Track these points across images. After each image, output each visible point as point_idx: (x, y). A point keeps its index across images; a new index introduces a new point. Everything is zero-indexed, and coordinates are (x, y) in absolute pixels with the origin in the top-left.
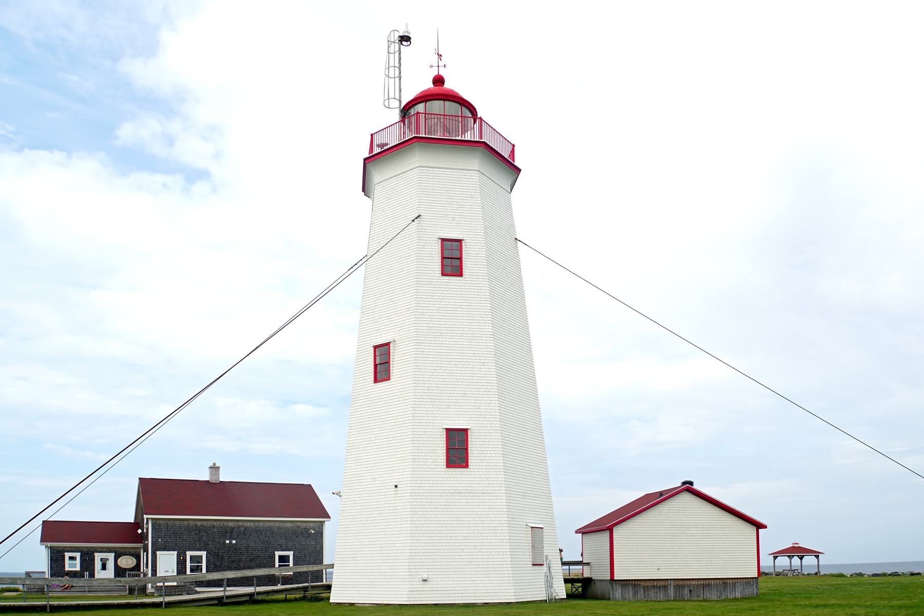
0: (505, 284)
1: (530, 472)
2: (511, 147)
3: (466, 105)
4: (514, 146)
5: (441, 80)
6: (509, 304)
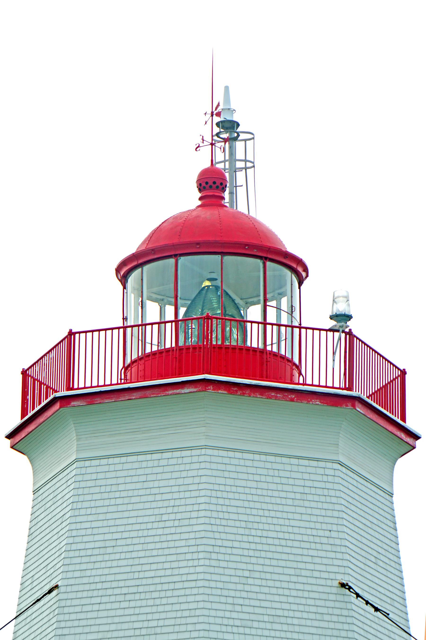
4: (404, 373)
5: (221, 184)
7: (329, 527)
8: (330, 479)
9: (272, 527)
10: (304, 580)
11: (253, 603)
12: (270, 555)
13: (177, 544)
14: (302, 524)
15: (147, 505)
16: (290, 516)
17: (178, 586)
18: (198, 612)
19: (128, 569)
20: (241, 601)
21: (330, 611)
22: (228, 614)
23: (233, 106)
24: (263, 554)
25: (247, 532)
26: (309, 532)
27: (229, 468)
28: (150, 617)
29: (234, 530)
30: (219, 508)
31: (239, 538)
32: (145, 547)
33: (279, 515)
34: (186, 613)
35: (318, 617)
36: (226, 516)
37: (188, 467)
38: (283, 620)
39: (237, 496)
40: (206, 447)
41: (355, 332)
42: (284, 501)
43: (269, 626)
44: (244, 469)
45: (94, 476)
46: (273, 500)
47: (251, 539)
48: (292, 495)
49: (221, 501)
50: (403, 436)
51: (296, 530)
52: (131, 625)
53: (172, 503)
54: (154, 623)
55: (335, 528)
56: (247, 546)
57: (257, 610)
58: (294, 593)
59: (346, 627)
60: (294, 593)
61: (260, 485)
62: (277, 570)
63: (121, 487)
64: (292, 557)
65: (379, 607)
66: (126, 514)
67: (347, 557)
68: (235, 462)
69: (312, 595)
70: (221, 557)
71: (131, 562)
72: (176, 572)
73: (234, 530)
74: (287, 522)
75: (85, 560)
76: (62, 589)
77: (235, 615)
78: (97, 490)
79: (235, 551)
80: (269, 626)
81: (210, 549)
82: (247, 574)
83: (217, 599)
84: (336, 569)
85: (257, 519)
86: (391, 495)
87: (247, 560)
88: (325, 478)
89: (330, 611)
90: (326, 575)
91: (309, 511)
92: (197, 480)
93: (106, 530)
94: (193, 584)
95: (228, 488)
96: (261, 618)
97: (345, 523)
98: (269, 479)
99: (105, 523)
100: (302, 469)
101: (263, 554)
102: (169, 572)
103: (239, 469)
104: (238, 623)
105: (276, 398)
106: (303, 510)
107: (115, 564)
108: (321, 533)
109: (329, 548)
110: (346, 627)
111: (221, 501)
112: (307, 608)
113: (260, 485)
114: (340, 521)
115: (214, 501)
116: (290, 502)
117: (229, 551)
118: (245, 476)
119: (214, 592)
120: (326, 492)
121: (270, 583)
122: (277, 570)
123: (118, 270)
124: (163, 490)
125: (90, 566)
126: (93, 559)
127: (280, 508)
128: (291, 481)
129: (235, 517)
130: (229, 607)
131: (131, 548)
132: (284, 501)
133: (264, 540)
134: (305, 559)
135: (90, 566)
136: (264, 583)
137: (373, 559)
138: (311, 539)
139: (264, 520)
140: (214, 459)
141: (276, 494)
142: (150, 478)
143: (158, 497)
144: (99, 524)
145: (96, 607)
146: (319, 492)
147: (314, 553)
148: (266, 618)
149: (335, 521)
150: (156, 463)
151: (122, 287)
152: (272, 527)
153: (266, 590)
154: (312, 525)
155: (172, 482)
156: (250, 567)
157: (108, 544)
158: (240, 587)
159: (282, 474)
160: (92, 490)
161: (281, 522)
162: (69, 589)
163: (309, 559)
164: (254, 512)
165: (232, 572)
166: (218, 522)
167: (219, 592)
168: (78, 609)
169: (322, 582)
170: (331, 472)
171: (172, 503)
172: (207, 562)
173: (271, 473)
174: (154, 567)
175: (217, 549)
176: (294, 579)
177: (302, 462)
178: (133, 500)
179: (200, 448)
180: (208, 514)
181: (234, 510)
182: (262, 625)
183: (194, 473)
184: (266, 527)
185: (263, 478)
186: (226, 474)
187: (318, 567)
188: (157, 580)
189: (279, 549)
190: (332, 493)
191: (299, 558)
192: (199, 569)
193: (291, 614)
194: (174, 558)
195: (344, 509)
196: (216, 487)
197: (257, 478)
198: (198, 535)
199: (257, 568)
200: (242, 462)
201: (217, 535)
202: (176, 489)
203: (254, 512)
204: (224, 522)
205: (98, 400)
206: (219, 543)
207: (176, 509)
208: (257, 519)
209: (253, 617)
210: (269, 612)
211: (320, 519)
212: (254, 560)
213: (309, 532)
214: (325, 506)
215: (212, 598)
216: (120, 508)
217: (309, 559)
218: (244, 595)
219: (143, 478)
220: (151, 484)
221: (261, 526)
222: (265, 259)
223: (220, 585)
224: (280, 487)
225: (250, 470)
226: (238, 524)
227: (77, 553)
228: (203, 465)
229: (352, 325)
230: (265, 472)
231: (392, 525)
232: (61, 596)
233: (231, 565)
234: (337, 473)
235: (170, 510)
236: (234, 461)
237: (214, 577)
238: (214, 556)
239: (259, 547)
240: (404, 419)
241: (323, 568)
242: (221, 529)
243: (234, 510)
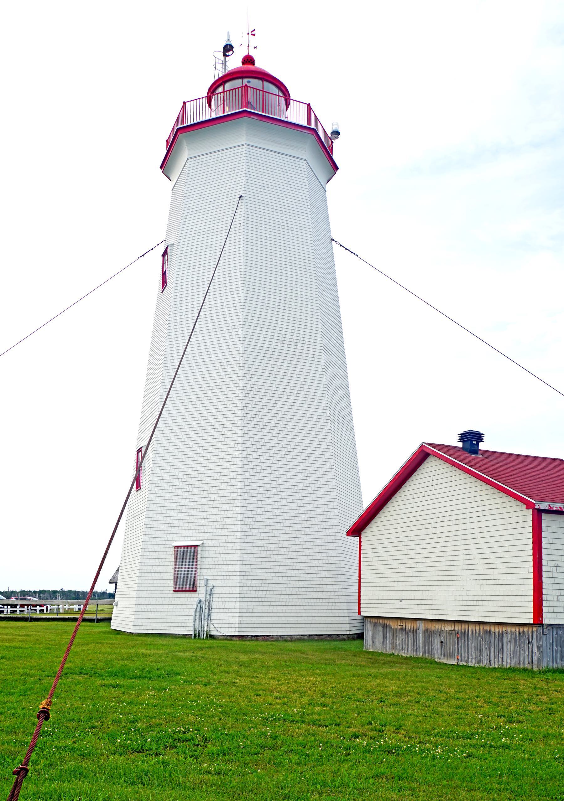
2: (305, 107)
4: (309, 105)
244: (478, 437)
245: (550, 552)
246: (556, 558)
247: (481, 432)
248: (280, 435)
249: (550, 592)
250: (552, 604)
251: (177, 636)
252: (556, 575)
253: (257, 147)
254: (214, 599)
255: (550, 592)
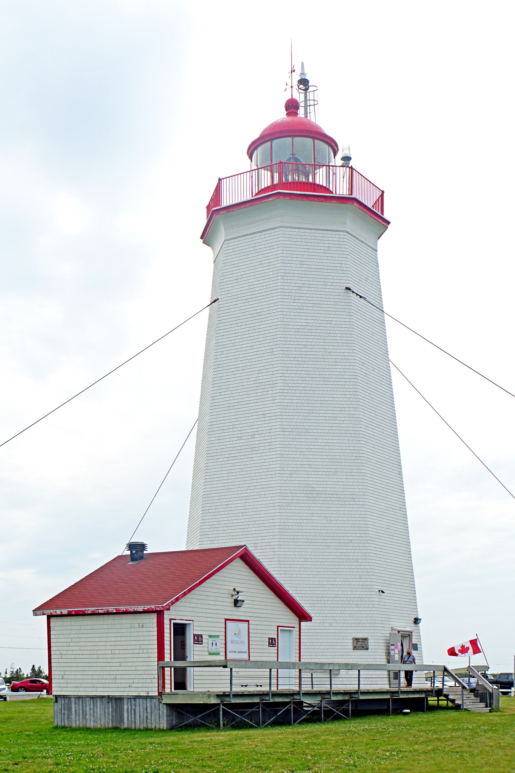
0: (375, 385)
1: (375, 499)
2: (380, 193)
3: (258, 144)
4: (383, 192)
5: (296, 106)
6: (382, 458)
7: (341, 262)
8: (342, 240)
9: (313, 263)
10: (329, 287)
11: (304, 298)
12: (312, 276)
13: (269, 274)
14: (328, 261)
15: (256, 258)
16: (322, 258)
17: (269, 293)
18: (278, 304)
19: (248, 288)
20: (298, 298)
21: (341, 300)
22: (292, 304)
23: (305, 72)
24: (309, 276)
25: (301, 266)
26: (331, 265)
27: (292, 236)
28: (257, 308)
29: (295, 266)
30: (288, 255)
31: (297, 269)
32: (255, 277)
33: (317, 257)
34: (273, 305)
35: (335, 303)
36: (291, 259)
37: (273, 237)
38: (318, 305)
39: (296, 250)
40: (281, 227)
41: (353, 167)
42: (319, 251)
43: (311, 308)
44: (300, 237)
45: (232, 247)
46: (314, 251)
47: (303, 269)
48: (323, 248)
49: (289, 252)
50: (381, 221)
51: (325, 264)
52: (249, 313)
53: (266, 255)
54: (259, 311)
55: (344, 262)
56: (301, 272)
57: (306, 302)
58: (324, 293)
59: (348, 307)
60: (324, 293)
61: (308, 244)
62: (316, 283)
63: (244, 251)
64: (323, 277)
65: (362, 296)
66: (246, 263)
67: (350, 276)
68: (296, 233)
69: (332, 294)
70: (289, 278)
71: (249, 284)
72: (268, 286)
73: (295, 266)
74: (321, 261)
75: (229, 286)
76: (220, 300)
77: (295, 304)
78: (234, 253)
79: (295, 275)
80: (311, 308)
81: (283, 274)
82: (301, 285)
83: (287, 297)
84: (344, 281)
85: (306, 260)
86: (376, 251)
87: (301, 279)
88: (340, 239)
89: (341, 300)
90: (339, 284)
91: (332, 255)
92: (277, 243)
93: (238, 271)
94: (275, 291)
95: (292, 246)
96: (308, 305)
97: (349, 260)
98: (312, 241)
99: (237, 268)
100: (328, 236)
101: (309, 276)
102: (265, 287)
103: (297, 237)
104: (296, 307)
105: (314, 201)
106: (329, 255)
107: (242, 286)
108: (337, 265)
109: (341, 272)
110: (348, 307)
111: (289, 252)
112: (330, 300)
113: (308, 244)
114: (347, 259)
115: (285, 252)
116: (322, 251)
117: (292, 275)
118: (300, 240)
119: (286, 294)
120: (340, 246)
121: (312, 289)
122: (316, 283)
123: (248, 153)
124: (262, 250)
125: (231, 288)
126: (233, 285)
127: (318, 254)
128: (323, 242)
129: (295, 259)
130: (292, 301)
131: (249, 278)
132: (319, 251)
133: (309, 270)
134: (329, 277)
135: (231, 288)
136: (309, 289)
137: (365, 279)
138: (332, 268)
139: (309, 260)
140: (285, 233)
141: (315, 248)
142: (257, 245)
143: (260, 253)
144: (235, 269)
145: (234, 307)
146: (337, 246)
147: (334, 274)
148: (310, 305)
149: (344, 259)
150: (259, 238)
151: (250, 161)
152: (313, 263)
153: (310, 292)
154: (333, 262)
155: (266, 246)
156: (303, 282)
157: (239, 277)
158: (298, 291)
159: (318, 238)
160: (232, 254)
161: (318, 261)
162: (223, 300)
163: (331, 277)
164: (305, 257)
165: (294, 285)
166: (287, 262)
167: (287, 294)
168: (226, 308)
169: (338, 288)
170: (343, 236)
171: (266, 255)
172: (282, 281)
173: (313, 238)
174: (259, 285)
175: (286, 275)
176: (324, 287)
177: (328, 232)
178: (250, 256)
179: (279, 227)
180: (282, 258)
181: (295, 256)
182: (308, 308)
183: (276, 240)
184: (311, 263)
185: (309, 241)
186: (291, 240)
187: (335, 281)
188: (260, 291)
189: (317, 273)
190: (343, 246)
191: (327, 277)
192: (278, 284)
193: (322, 303)
194: (267, 280)
195: (348, 253)
196: (286, 246)
197: (306, 241)
198: (278, 269)
199: (306, 282)
200: (299, 234)
201: (287, 268)
202: (268, 248)
203: (305, 257)
204: (290, 262)
205: (231, 209)
206: (288, 271)
207: (268, 258)
208: (306, 260)
209: (304, 305)
210: (312, 302)
211: (337, 259)
212: (304, 279)
213: (331, 265)
214: (340, 252)
215: (284, 297)
216: (244, 260)
217: (331, 277)
218: (300, 295)
219: (254, 245)
220: (257, 248)
221: (308, 263)
222: (314, 138)
223: (288, 291)
224: (317, 245)
225: (303, 237)
226: (297, 262)
227: (226, 283)
228: (280, 236)
229: (352, 163)
230: (310, 238)
231: (376, 264)
232: (220, 303)
233: (293, 281)
234: (346, 237)
235: (265, 259)
236: (295, 233)
237: (285, 287)
238: (285, 278)
239: (307, 273)
240: (382, 213)
241: (338, 281)
242: (289, 265)
243: (295, 256)
244: (142, 546)
245: (57, 644)
246: (60, 648)
247: (145, 543)
248: (232, 531)
249: (57, 673)
250: (58, 681)
251: (370, 668)
252: (61, 660)
253: (311, 229)
254: (384, 648)
255: (57, 673)
